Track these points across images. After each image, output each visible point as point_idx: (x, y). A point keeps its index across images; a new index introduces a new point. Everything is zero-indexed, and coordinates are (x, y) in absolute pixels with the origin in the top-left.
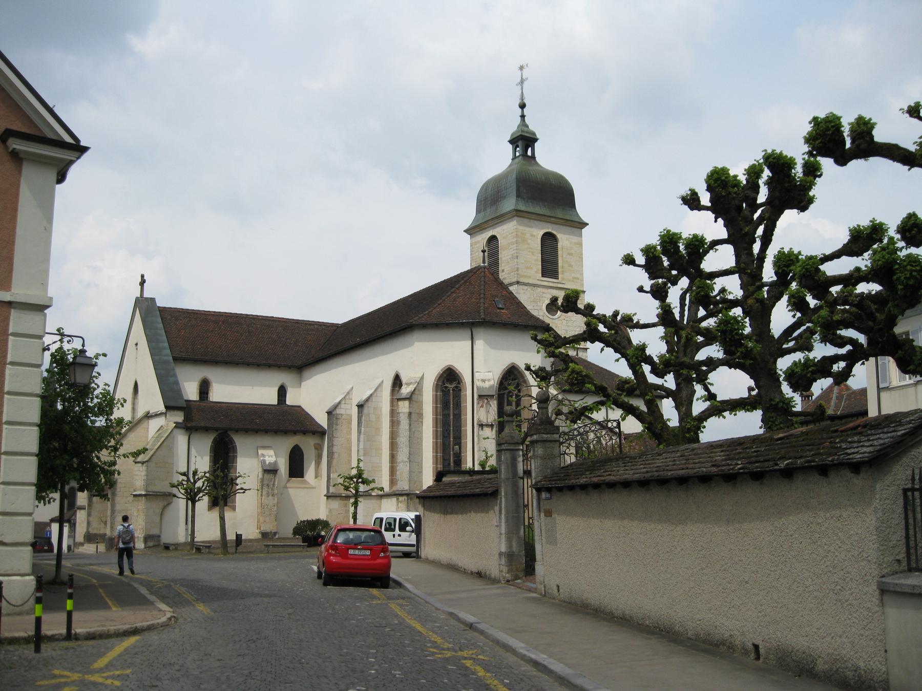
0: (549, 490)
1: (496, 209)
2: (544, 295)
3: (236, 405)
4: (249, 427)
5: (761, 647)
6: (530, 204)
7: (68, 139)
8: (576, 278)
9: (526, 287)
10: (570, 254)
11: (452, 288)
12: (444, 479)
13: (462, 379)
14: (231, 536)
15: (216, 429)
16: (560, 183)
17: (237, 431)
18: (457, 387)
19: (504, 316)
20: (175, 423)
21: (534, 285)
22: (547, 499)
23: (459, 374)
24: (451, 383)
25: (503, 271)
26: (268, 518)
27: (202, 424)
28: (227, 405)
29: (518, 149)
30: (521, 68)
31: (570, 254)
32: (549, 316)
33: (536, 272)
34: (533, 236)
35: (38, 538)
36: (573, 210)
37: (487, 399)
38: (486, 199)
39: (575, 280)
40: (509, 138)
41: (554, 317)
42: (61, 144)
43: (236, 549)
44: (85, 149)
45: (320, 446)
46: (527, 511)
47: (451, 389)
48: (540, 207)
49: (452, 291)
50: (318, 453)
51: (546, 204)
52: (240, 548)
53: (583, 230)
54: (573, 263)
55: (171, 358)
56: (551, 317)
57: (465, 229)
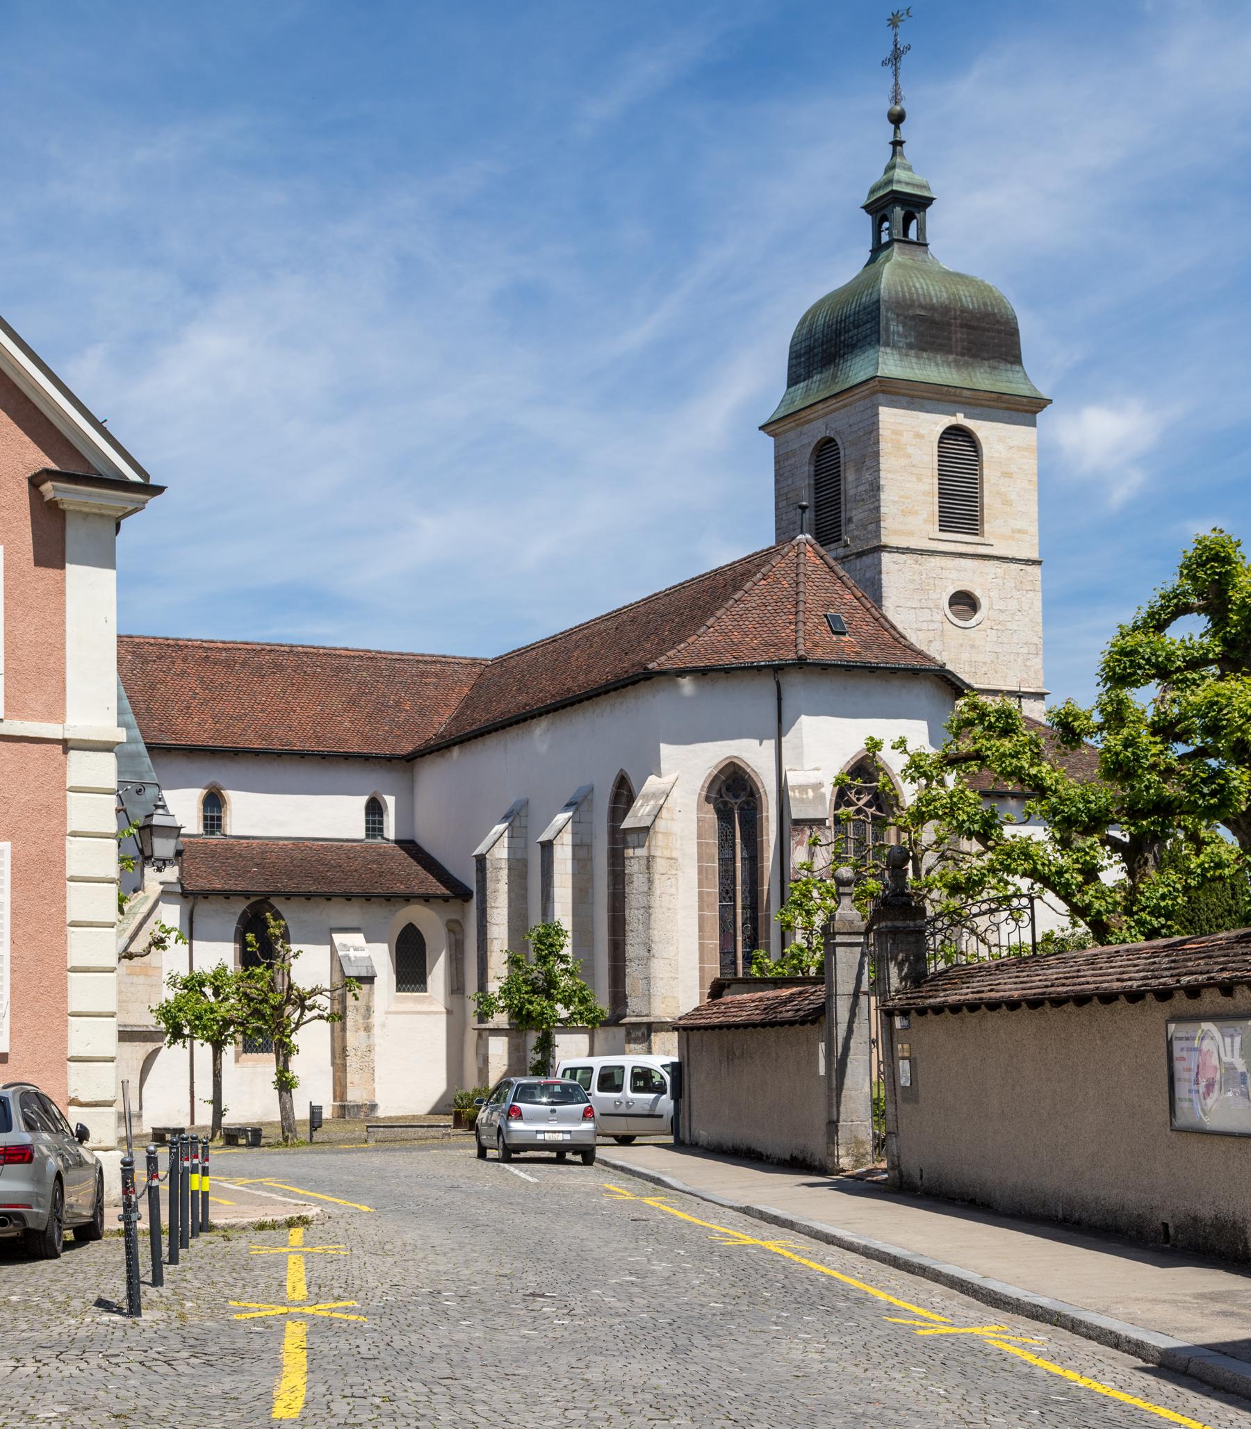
0: (905, 1013)
1: (834, 377)
2: (945, 573)
3: (281, 842)
4: (312, 889)
5: (1170, 1225)
6: (914, 360)
7: (133, 476)
8: (1019, 531)
9: (904, 557)
10: (1007, 475)
11: (736, 589)
12: (727, 998)
13: (759, 785)
14: (301, 1113)
15: (246, 895)
16: (985, 304)
17: (288, 896)
18: (747, 803)
19: (847, 650)
20: (161, 883)
21: (922, 552)
22: (904, 1029)
23: (753, 775)
24: (736, 797)
25: (850, 520)
26: (358, 1076)
27: (218, 886)
28: (261, 842)
29: (886, 225)
30: (894, 22)
31: (1007, 475)
32: (956, 621)
33: (925, 521)
34: (919, 436)
35: (910, 932)
36: (1017, 368)
37: (811, 828)
38: (810, 350)
39: (1017, 536)
40: (864, 199)
41: (967, 624)
42: (123, 484)
43: (311, 1136)
44: (159, 490)
45: (460, 925)
46: (875, 1050)
47: (736, 807)
48: (937, 365)
49: (736, 597)
50: (456, 940)
51: (951, 357)
52: (318, 1136)
53: (1038, 415)
54: (1013, 496)
55: (142, 748)
56: (961, 623)
57: (761, 424)
